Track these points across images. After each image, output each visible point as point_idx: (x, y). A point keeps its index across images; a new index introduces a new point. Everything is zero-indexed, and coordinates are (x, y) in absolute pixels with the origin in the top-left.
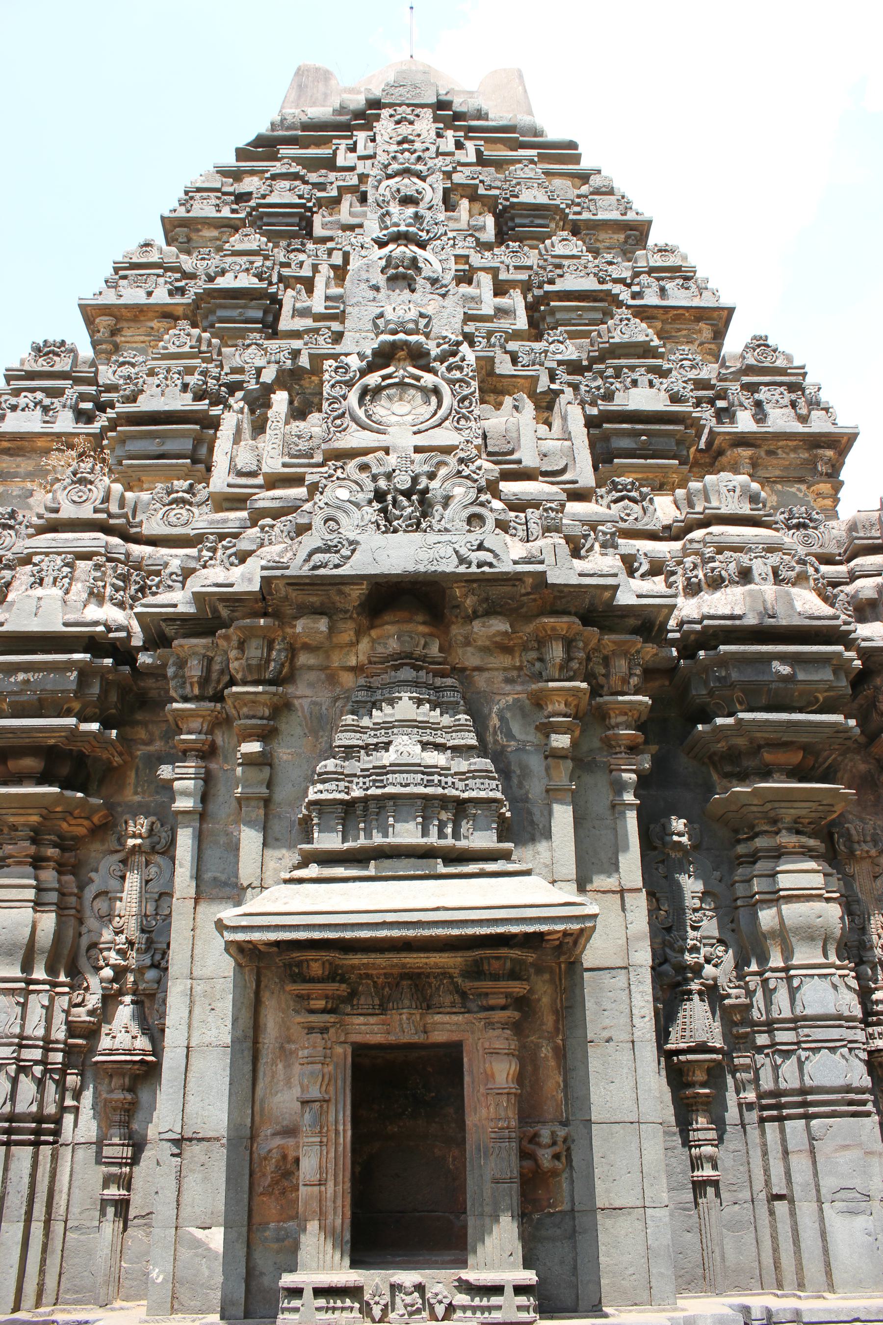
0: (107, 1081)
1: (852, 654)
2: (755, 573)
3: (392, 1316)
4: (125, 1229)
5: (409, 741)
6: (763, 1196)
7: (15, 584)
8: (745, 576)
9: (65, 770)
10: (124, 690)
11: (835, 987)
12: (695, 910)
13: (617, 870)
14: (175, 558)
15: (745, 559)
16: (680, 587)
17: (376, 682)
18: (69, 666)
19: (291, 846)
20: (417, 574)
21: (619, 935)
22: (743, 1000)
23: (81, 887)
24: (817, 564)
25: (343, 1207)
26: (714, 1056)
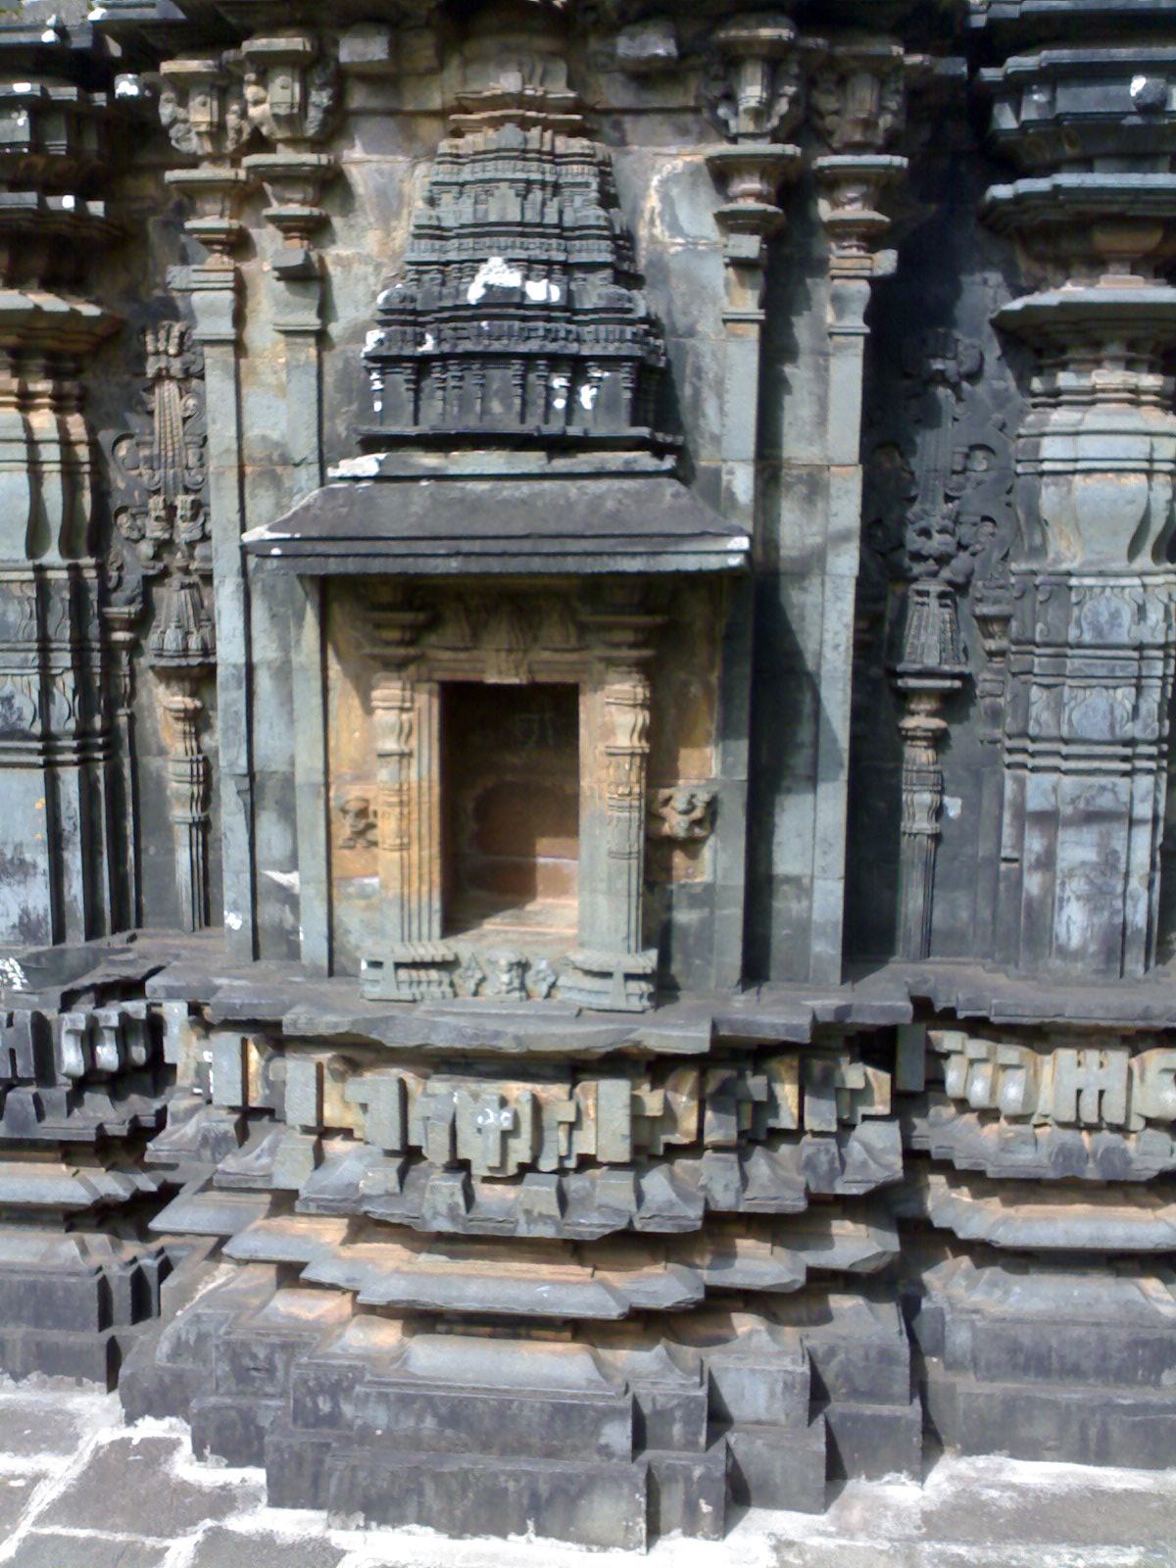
25: (430, 873)
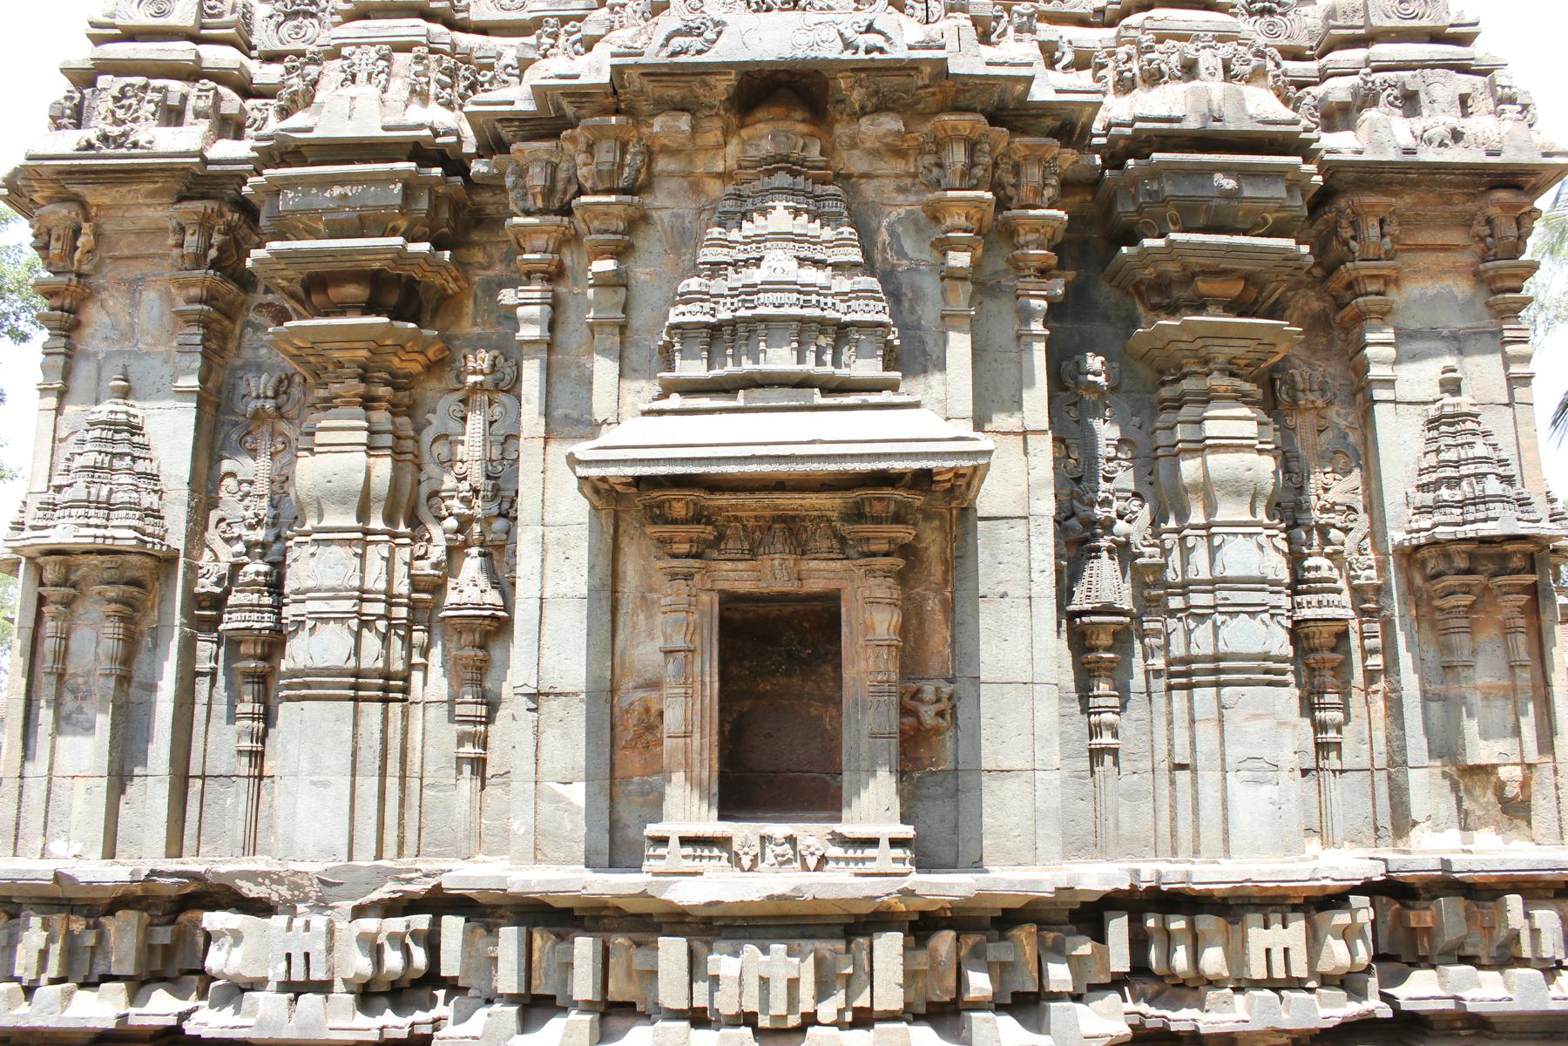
0: (455, 638)
1: (1312, 168)
2: (1202, 66)
3: (761, 865)
4: (483, 787)
5: (783, 255)
6: (1165, 766)
7: (323, 82)
8: (1189, 69)
9: (393, 299)
10: (456, 207)
11: (1261, 547)
12: (1109, 460)
13: (1020, 408)
14: (509, 49)
15: (1190, 49)
16: (1111, 84)
17: (746, 190)
18: (392, 177)
19: (650, 377)
20: (794, 61)
21: (1018, 481)
22: (1157, 560)
23: (418, 431)
24: (1278, 57)
26: (1121, 619)
